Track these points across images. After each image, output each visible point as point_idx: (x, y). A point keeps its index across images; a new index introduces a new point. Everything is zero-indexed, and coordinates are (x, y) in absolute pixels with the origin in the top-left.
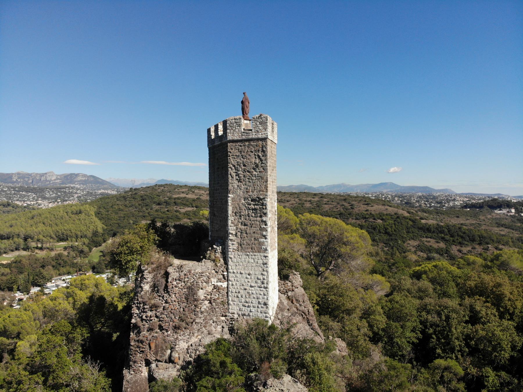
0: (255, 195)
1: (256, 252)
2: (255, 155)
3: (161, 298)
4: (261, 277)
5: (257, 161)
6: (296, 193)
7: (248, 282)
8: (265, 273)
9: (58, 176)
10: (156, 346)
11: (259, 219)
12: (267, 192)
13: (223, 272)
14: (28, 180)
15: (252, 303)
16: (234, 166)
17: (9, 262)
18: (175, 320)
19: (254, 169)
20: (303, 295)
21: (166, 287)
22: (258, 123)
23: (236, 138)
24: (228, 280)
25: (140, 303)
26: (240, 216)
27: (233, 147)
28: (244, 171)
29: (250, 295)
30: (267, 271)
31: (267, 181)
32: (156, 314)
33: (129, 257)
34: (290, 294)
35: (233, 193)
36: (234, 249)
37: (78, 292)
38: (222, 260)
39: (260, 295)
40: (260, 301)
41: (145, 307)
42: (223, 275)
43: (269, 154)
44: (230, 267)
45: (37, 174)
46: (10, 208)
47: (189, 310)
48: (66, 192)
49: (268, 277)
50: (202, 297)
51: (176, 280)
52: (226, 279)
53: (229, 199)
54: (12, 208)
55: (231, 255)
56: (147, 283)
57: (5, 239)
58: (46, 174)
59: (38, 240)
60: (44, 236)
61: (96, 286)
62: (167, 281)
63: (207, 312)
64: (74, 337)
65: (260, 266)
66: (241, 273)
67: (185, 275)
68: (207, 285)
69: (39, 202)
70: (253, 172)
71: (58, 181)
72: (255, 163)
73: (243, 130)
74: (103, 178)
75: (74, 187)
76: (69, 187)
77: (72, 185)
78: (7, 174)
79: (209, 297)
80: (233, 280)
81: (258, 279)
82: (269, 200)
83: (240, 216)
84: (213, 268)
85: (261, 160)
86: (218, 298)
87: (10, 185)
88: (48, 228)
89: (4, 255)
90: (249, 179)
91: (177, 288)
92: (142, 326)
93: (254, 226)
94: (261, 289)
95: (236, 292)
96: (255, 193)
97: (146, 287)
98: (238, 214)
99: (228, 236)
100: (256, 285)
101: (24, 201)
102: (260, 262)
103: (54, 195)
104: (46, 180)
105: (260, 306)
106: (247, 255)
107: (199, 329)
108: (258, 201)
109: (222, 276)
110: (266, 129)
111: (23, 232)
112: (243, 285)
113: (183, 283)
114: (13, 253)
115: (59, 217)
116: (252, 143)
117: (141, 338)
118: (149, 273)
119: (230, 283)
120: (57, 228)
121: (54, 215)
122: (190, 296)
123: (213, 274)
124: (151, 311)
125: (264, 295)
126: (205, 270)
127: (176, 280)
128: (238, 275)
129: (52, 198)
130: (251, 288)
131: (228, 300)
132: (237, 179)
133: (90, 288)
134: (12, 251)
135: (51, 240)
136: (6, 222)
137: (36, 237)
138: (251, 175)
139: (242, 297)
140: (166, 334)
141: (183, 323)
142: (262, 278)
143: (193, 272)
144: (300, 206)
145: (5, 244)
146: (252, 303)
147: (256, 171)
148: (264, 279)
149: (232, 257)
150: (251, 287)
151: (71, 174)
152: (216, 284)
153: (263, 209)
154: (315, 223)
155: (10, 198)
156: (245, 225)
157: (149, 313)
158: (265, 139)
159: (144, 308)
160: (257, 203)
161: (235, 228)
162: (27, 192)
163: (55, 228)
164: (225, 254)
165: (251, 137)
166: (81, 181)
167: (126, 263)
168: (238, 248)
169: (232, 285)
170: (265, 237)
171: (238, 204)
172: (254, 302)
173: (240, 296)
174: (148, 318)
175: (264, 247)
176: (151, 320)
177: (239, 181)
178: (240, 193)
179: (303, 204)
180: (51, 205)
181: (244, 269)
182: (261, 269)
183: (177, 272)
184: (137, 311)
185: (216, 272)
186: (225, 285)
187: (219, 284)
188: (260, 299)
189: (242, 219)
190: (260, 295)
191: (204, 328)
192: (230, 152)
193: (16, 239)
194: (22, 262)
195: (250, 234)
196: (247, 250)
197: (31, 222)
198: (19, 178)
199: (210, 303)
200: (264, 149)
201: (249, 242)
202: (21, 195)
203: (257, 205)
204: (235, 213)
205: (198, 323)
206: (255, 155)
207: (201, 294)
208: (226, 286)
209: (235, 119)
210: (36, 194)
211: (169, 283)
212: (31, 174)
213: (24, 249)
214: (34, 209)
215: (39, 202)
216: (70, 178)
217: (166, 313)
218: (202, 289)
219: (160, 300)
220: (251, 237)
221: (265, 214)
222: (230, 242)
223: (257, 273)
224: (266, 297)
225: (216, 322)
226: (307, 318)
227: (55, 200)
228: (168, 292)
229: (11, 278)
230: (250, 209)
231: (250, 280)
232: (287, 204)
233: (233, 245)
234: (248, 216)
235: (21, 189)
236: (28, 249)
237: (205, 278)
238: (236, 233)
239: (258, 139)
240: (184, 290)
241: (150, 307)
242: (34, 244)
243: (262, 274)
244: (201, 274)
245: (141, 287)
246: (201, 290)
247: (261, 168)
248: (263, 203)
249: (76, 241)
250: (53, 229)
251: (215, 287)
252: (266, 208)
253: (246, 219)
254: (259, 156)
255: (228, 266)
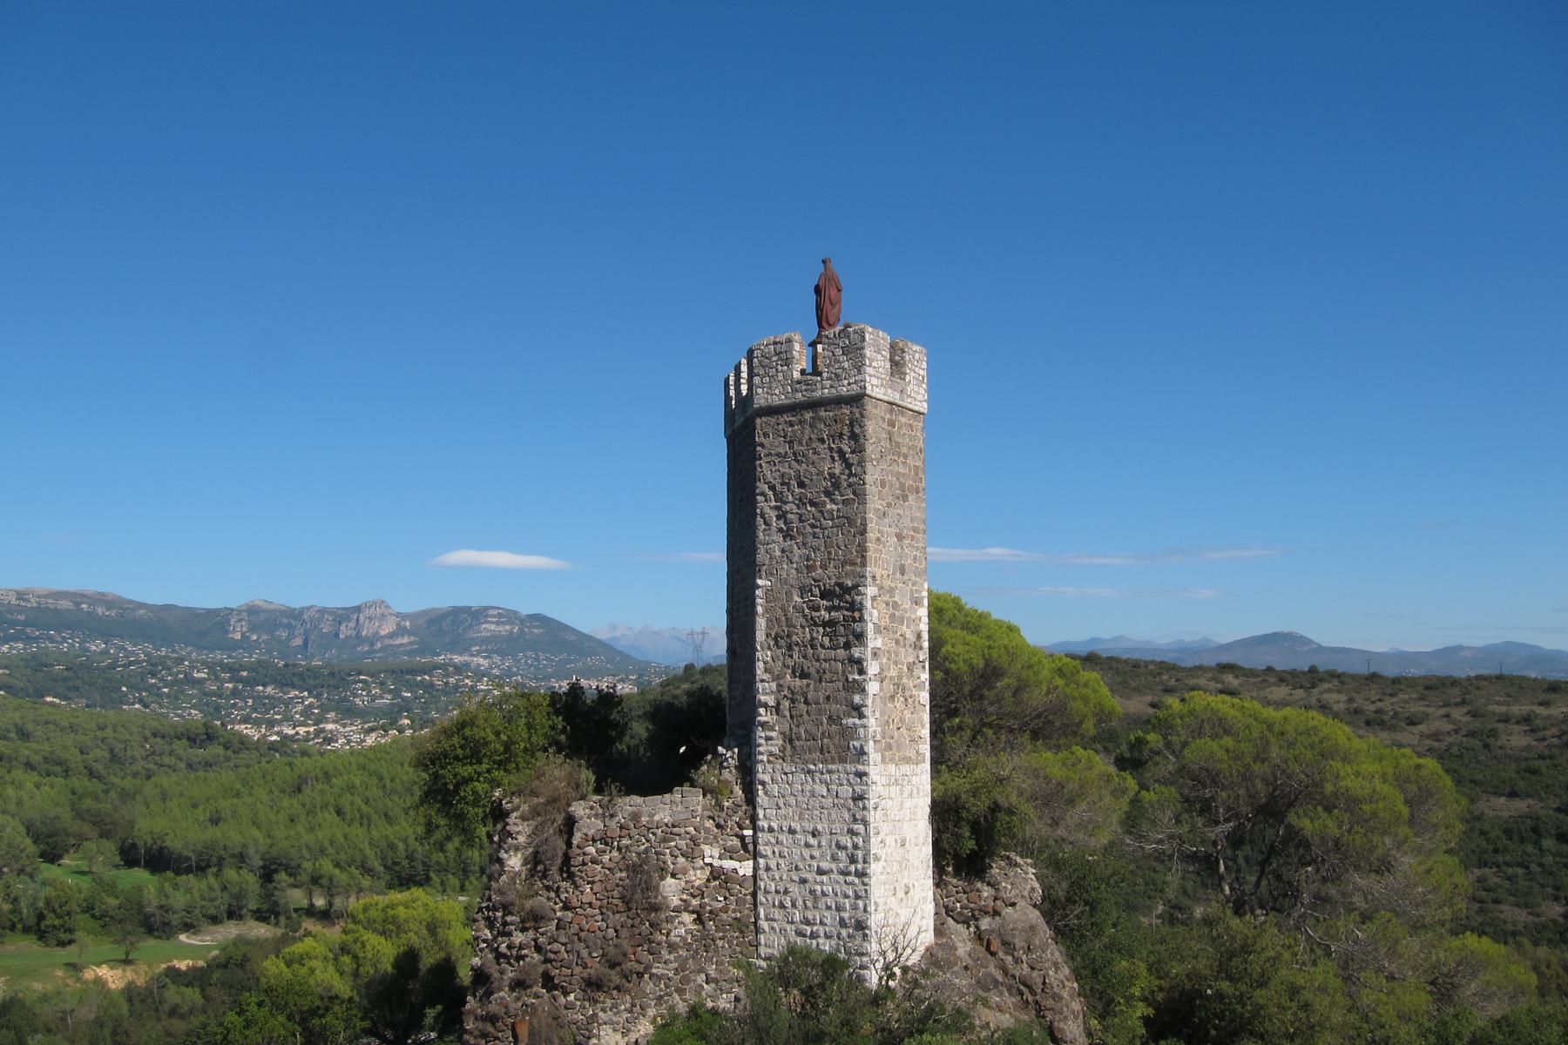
0: (829, 577)
1: (833, 762)
2: (831, 449)
3: (553, 895)
4: (847, 841)
5: (838, 468)
6: (1454, 682)
7: (812, 857)
8: (860, 828)
9: (404, 617)
10: (531, 1034)
11: (841, 653)
12: (864, 565)
13: (741, 828)
14: (289, 638)
15: (822, 923)
16: (772, 488)
17: (201, 963)
18: (589, 961)
19: (828, 494)
20: (1032, 928)
21: (567, 859)
22: (839, 352)
23: (778, 399)
24: (755, 855)
25: (495, 909)
26: (790, 648)
27: (769, 430)
28: (801, 502)
29: (816, 899)
30: (865, 823)
31: (863, 532)
32: (535, 940)
33: (470, 769)
34: (985, 923)
35: (769, 574)
36: (771, 754)
37: (373, 939)
38: (738, 791)
39: (846, 896)
40: (846, 915)
41: (509, 919)
42: (742, 838)
43: (871, 450)
44: (761, 813)
45: (323, 611)
46: (216, 750)
47: (632, 936)
48: (433, 685)
49: (867, 840)
50: (675, 901)
51: (594, 841)
52: (750, 850)
53: (758, 592)
54: (220, 750)
55: (763, 774)
56: (517, 849)
57: (188, 871)
58: (358, 609)
59: (315, 880)
60: (338, 865)
61: (432, 928)
62: (569, 844)
63: (688, 947)
64: (323, 1027)
65: (843, 806)
66: (792, 831)
67: (621, 827)
68: (689, 866)
69: (330, 727)
70: (824, 504)
71: (406, 640)
72: (832, 475)
73: (796, 375)
74: (585, 629)
75: (467, 664)
76: (444, 666)
77: (457, 659)
78: (209, 612)
79: (695, 902)
80: (769, 853)
81: (839, 846)
82: (871, 591)
83: (790, 648)
84: (707, 813)
85: (849, 466)
86: (725, 910)
87: (219, 656)
88: (357, 831)
89: (183, 937)
90: (813, 526)
91: (599, 867)
92: (497, 975)
93: (828, 676)
94: (850, 879)
95: (777, 892)
96: (831, 570)
97: (514, 862)
98: (782, 643)
99: (755, 714)
100: (833, 866)
101: (271, 724)
102: (846, 791)
103: (387, 700)
104: (358, 635)
105: (844, 933)
106: (809, 772)
107: (661, 997)
108: (840, 597)
109: (736, 842)
110: (859, 368)
111: (256, 841)
112: (797, 868)
113: (615, 853)
114: (220, 928)
115: (399, 787)
116: (822, 414)
117: (493, 1008)
118: (523, 818)
119: (761, 861)
120: (390, 831)
121: (381, 778)
122: (637, 895)
123: (707, 830)
124: (524, 930)
125: (857, 897)
126: (682, 816)
127: (594, 841)
128: (783, 837)
129: (378, 713)
130: (818, 878)
131: (757, 918)
132: (781, 530)
133: (411, 934)
134: (215, 920)
135: (366, 882)
136: (195, 806)
137: (308, 865)
138: (818, 515)
139: (794, 905)
140: (562, 1000)
141: (613, 972)
142: (849, 845)
143: (644, 819)
144: (1476, 743)
145: (189, 891)
146: (822, 923)
147: (833, 501)
148: (855, 847)
149: (767, 778)
150: (821, 872)
151: (456, 611)
152: (716, 863)
153: (854, 620)
154: (1222, 727)
155: (218, 708)
156: (804, 675)
157: (518, 938)
158: (858, 399)
159: (505, 924)
160: (836, 602)
161: (774, 685)
162: (284, 683)
163: (381, 830)
164: (747, 771)
165: (818, 394)
166: (495, 638)
167: (457, 786)
168: (783, 750)
169: (768, 869)
170: (858, 711)
171: (783, 609)
172: (828, 921)
173: (789, 904)
174: (514, 952)
175: (857, 744)
176: (523, 957)
177: (787, 535)
178: (789, 571)
179: (1493, 733)
180: (370, 740)
181: (801, 817)
182: (846, 816)
183: (596, 816)
184: (487, 932)
185: (718, 826)
186: (746, 868)
187: (728, 864)
188: (844, 910)
189: (795, 656)
190: (846, 896)
191: (675, 995)
192: (762, 445)
193: (231, 874)
194: (248, 966)
195: (817, 703)
196: (807, 756)
197: (289, 804)
198: (253, 629)
199: (699, 920)
200: (857, 430)
201: (814, 730)
202: (258, 698)
203: (837, 609)
204: (775, 639)
205: (659, 978)
206: (831, 449)
207: (671, 890)
208: (749, 873)
209: (775, 343)
210: (318, 697)
211: (575, 851)
212: (302, 610)
213: (261, 916)
214: (304, 753)
215: (330, 727)
216: (451, 626)
217: (564, 940)
218: (673, 876)
219: (549, 899)
220: (820, 712)
221: (860, 637)
222: (760, 733)
223: (836, 827)
224: (861, 903)
225: (716, 981)
226: (1037, 1002)
227: (390, 719)
228: (571, 876)
229: (204, 1026)
230: (816, 624)
231: (816, 853)
232: (1409, 736)
233: (768, 743)
234: (813, 647)
235: (262, 673)
236: (277, 915)
237: (682, 843)
238: (778, 704)
239: (839, 401)
240: (619, 875)
241: (523, 921)
242: (297, 897)
243: (852, 832)
244: (670, 831)
245: (500, 861)
246: (670, 880)
247: (849, 491)
248: (853, 603)
249: (462, 889)
250: (374, 833)
251: (715, 873)
252: (861, 619)
253: (805, 657)
254: (841, 453)
255: (754, 808)
